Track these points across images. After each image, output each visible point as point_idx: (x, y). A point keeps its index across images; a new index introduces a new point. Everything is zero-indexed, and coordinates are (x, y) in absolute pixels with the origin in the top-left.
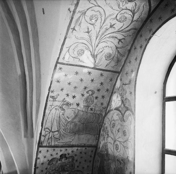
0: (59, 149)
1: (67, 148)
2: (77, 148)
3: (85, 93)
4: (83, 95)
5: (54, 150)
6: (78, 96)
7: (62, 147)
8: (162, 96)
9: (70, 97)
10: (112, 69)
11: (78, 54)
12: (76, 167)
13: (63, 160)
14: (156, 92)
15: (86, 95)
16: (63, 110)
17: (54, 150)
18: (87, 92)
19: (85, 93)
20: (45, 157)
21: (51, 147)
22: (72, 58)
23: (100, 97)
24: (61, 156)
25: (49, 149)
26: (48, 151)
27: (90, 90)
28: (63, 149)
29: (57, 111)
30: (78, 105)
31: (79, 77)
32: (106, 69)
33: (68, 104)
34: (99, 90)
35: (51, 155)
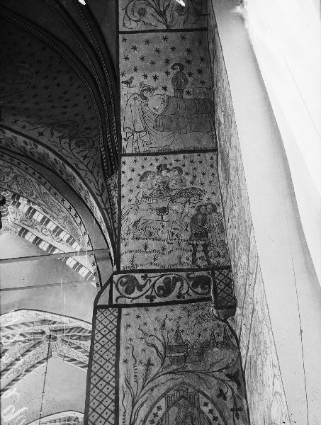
0: (154, 158)
1: (167, 156)
2: (182, 155)
3: (170, 70)
4: (168, 73)
5: (145, 159)
6: (161, 75)
7: (157, 154)
8: (229, 115)
9: (150, 78)
10: (195, 27)
11: (140, 15)
12: (188, 183)
13: (164, 173)
14: (135, 161)
15: (173, 73)
16: (146, 98)
17: (145, 159)
18: (173, 68)
19: (170, 70)
20: (133, 170)
21: (139, 154)
22: (134, 23)
23: (194, 72)
24: (158, 167)
25: (138, 158)
26: (135, 161)
27: (176, 64)
28: (160, 158)
29: (137, 101)
30: (165, 88)
31: (152, 47)
32: (185, 27)
33: (150, 89)
34: (188, 62)
35: (143, 167)
